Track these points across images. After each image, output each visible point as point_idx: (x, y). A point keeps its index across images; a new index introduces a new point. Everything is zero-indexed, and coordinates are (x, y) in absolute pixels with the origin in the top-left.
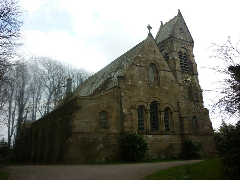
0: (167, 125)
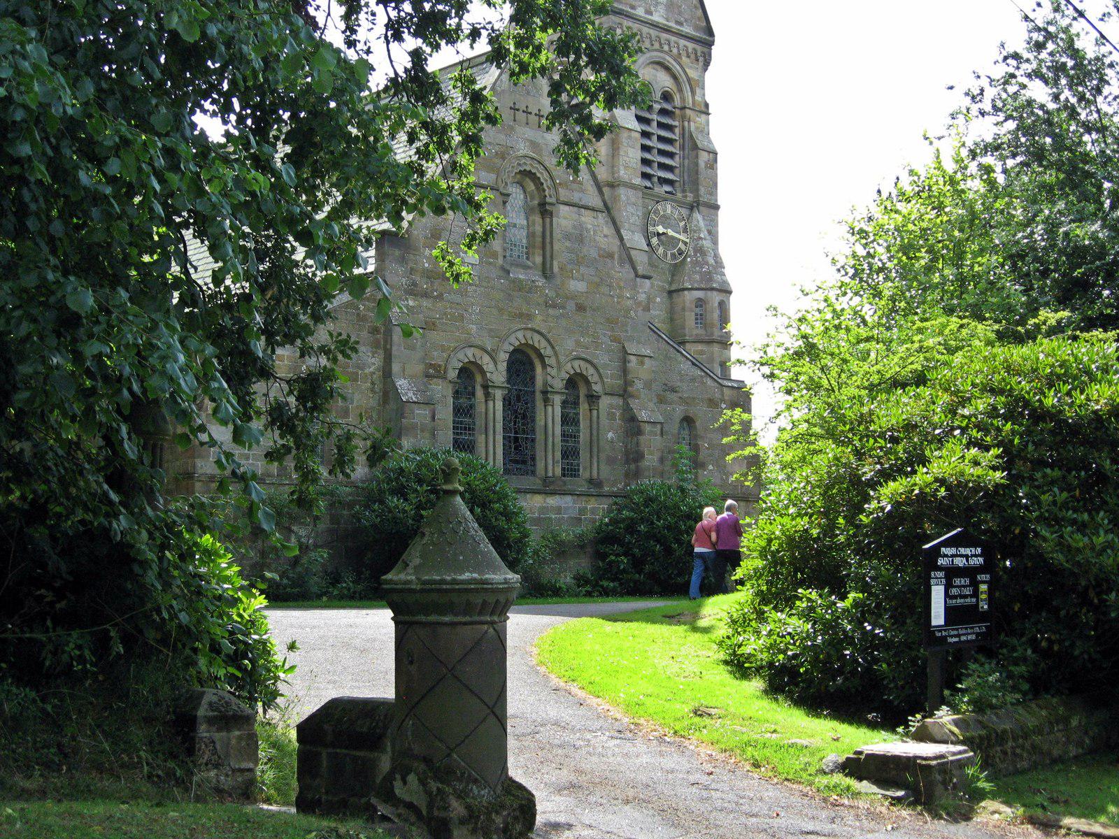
0: (569, 454)
